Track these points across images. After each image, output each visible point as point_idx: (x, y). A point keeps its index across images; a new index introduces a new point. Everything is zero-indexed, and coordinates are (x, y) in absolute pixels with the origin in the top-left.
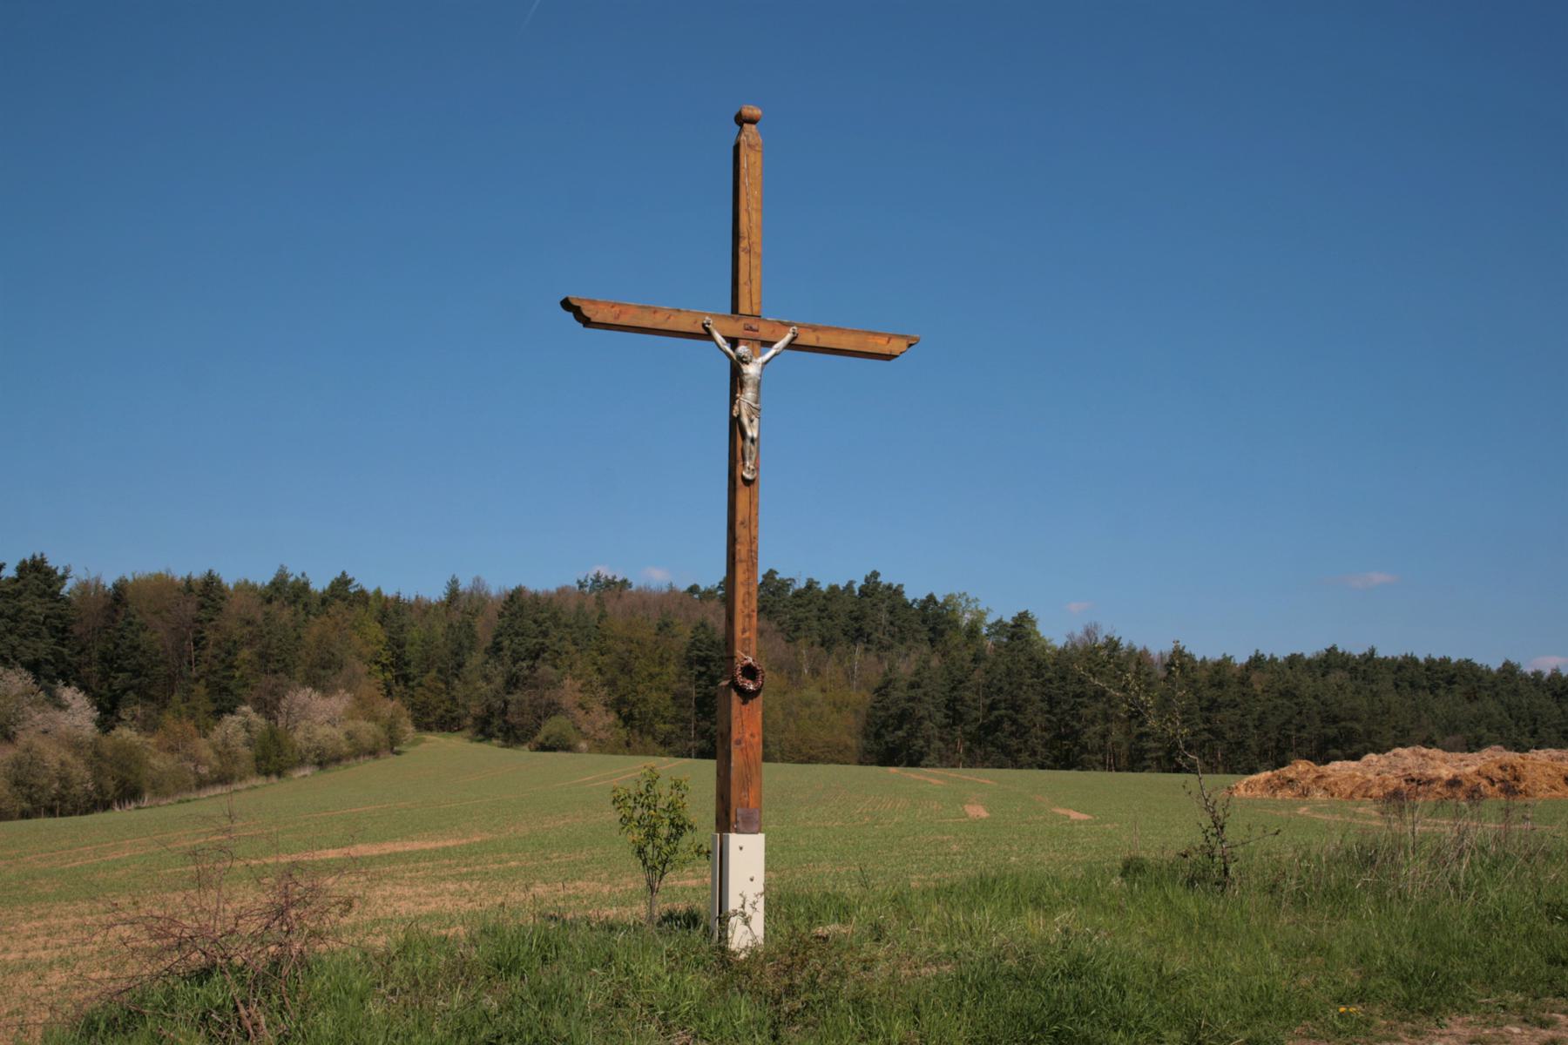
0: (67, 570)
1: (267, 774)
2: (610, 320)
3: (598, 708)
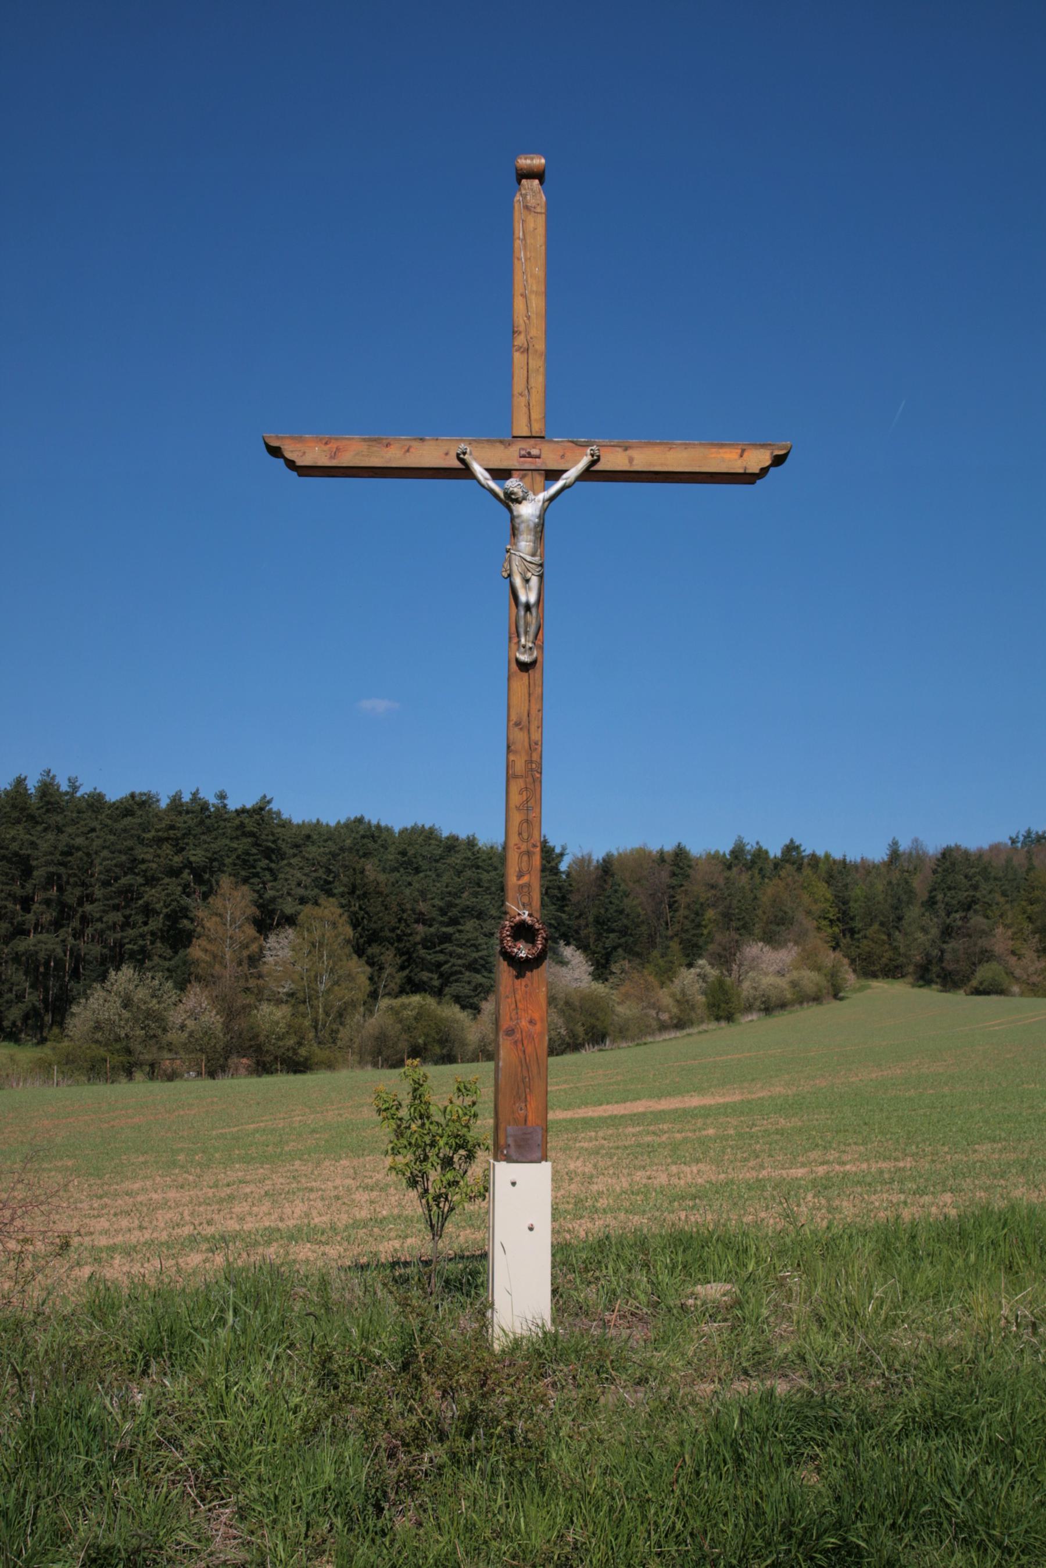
0: (564, 848)
1: (718, 1019)
2: (324, 461)
3: (1029, 954)
